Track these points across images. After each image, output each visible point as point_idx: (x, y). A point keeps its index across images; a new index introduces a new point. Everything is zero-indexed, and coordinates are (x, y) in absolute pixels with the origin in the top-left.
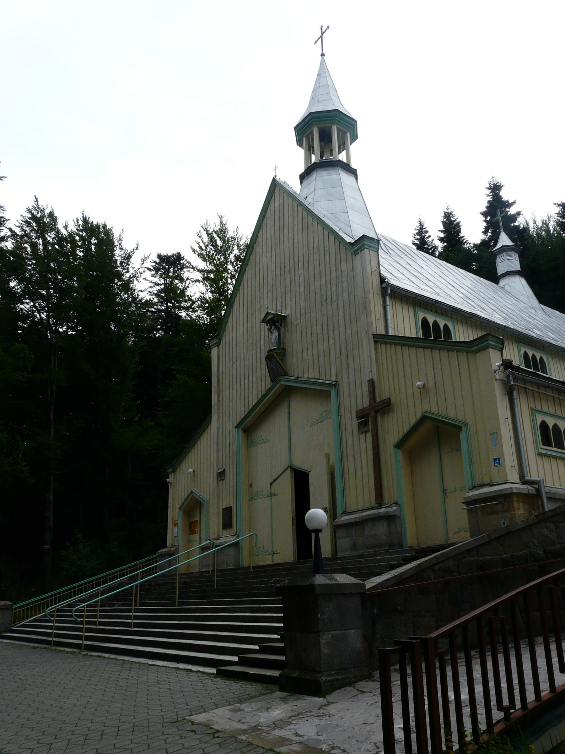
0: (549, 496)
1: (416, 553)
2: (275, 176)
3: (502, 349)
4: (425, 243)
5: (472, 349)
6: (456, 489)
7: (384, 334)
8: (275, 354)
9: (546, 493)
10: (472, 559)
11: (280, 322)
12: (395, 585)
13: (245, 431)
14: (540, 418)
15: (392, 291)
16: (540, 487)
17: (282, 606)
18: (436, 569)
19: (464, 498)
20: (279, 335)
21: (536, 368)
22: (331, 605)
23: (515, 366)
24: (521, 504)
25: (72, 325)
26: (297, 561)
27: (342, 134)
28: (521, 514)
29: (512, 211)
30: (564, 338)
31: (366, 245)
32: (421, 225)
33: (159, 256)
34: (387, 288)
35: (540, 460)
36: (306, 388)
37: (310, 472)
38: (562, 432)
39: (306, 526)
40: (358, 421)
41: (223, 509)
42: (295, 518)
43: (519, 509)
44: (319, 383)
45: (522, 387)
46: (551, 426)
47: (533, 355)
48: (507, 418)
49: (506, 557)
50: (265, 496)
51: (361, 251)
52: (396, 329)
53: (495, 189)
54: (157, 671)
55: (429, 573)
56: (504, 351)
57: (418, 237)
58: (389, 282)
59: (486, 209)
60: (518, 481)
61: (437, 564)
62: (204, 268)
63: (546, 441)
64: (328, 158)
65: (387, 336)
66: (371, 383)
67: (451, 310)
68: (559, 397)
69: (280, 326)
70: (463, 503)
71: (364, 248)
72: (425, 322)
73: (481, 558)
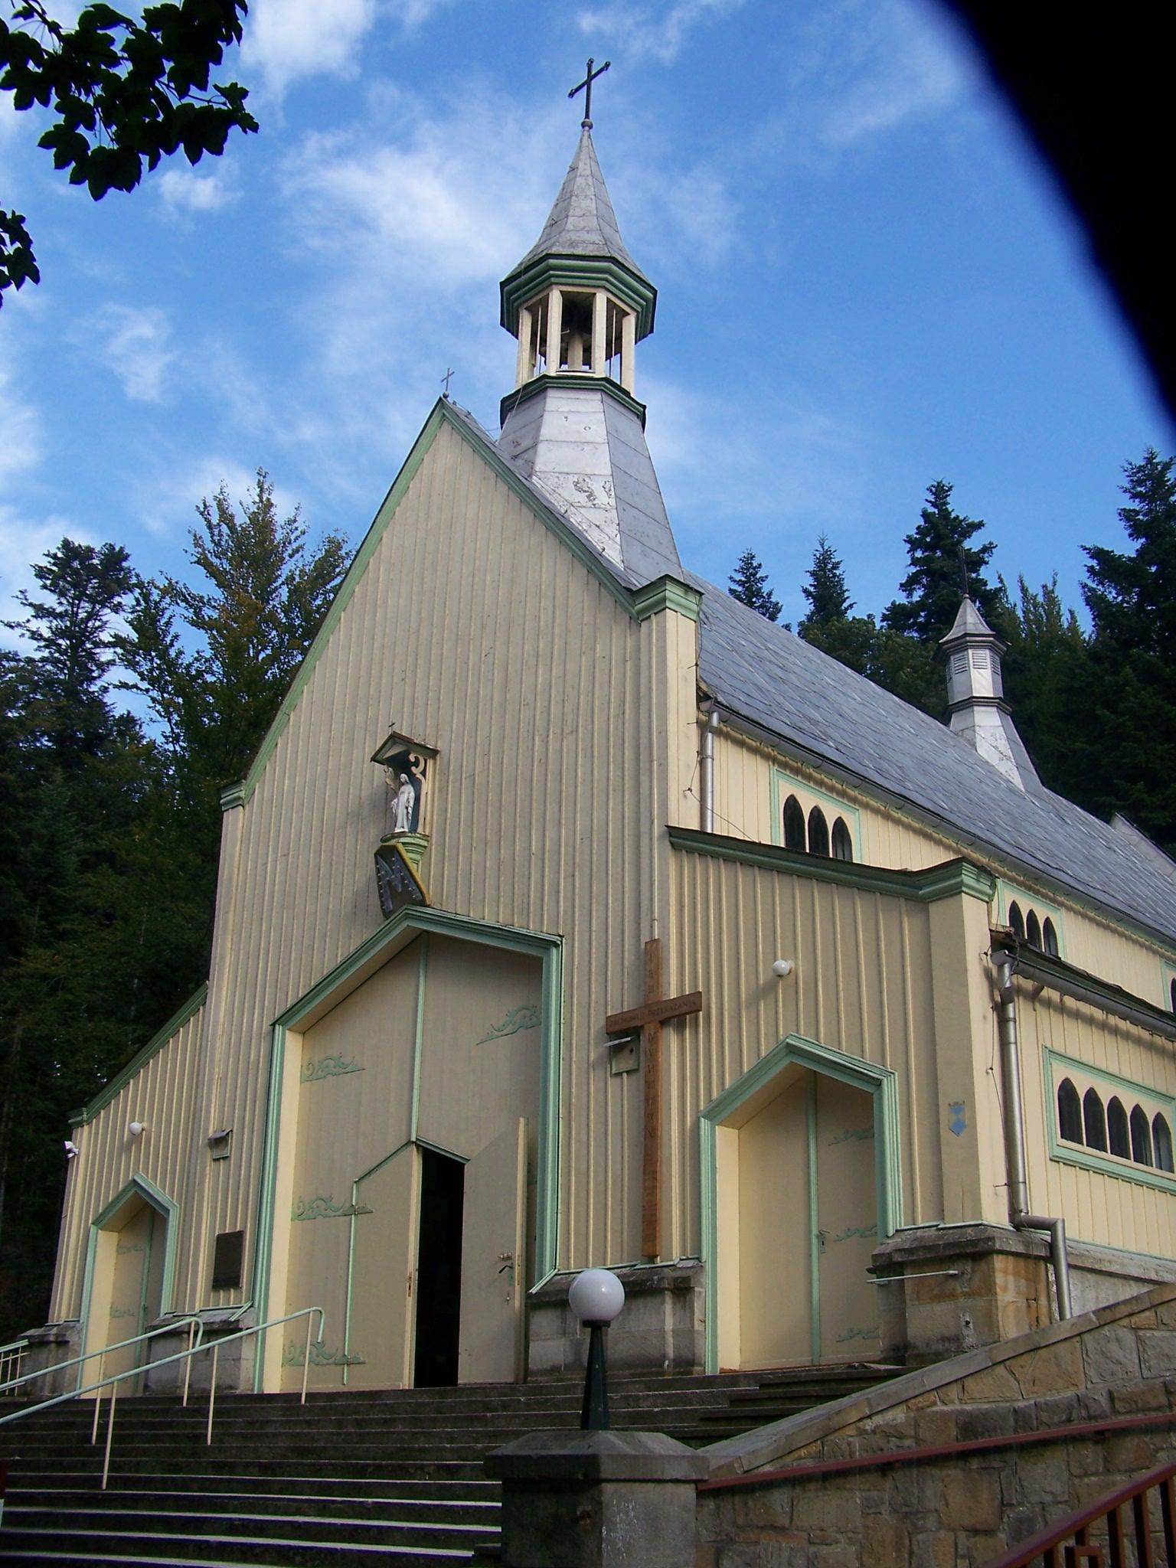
0: (1073, 1262)
1: (762, 1386)
2: (446, 396)
3: (991, 898)
4: (758, 593)
5: (920, 892)
6: (849, 1233)
8: (401, 847)
10: (945, 1408)
14: (1060, 1072)
16: (1054, 1236)
17: (500, 1504)
18: (866, 1431)
19: (874, 1256)
20: (417, 799)
22: (631, 1507)
24: (1011, 1279)
28: (1009, 1303)
29: (973, 544)
30: (1175, 907)
31: (672, 601)
32: (1085, 549)
36: (463, 941)
37: (468, 1160)
38: (1126, 1116)
40: (611, 1043)
43: (1005, 1289)
44: (534, 940)
47: (1031, 914)
48: (992, 1069)
49: (1025, 1406)
50: (338, 1213)
53: (940, 493)
55: (850, 1439)
56: (994, 904)
57: (739, 577)
59: (52, 129)
62: (177, 583)
63: (1069, 1130)
65: (701, 835)
69: (419, 776)
70: (870, 1271)
71: (663, 607)
72: (792, 808)
73: (968, 1407)
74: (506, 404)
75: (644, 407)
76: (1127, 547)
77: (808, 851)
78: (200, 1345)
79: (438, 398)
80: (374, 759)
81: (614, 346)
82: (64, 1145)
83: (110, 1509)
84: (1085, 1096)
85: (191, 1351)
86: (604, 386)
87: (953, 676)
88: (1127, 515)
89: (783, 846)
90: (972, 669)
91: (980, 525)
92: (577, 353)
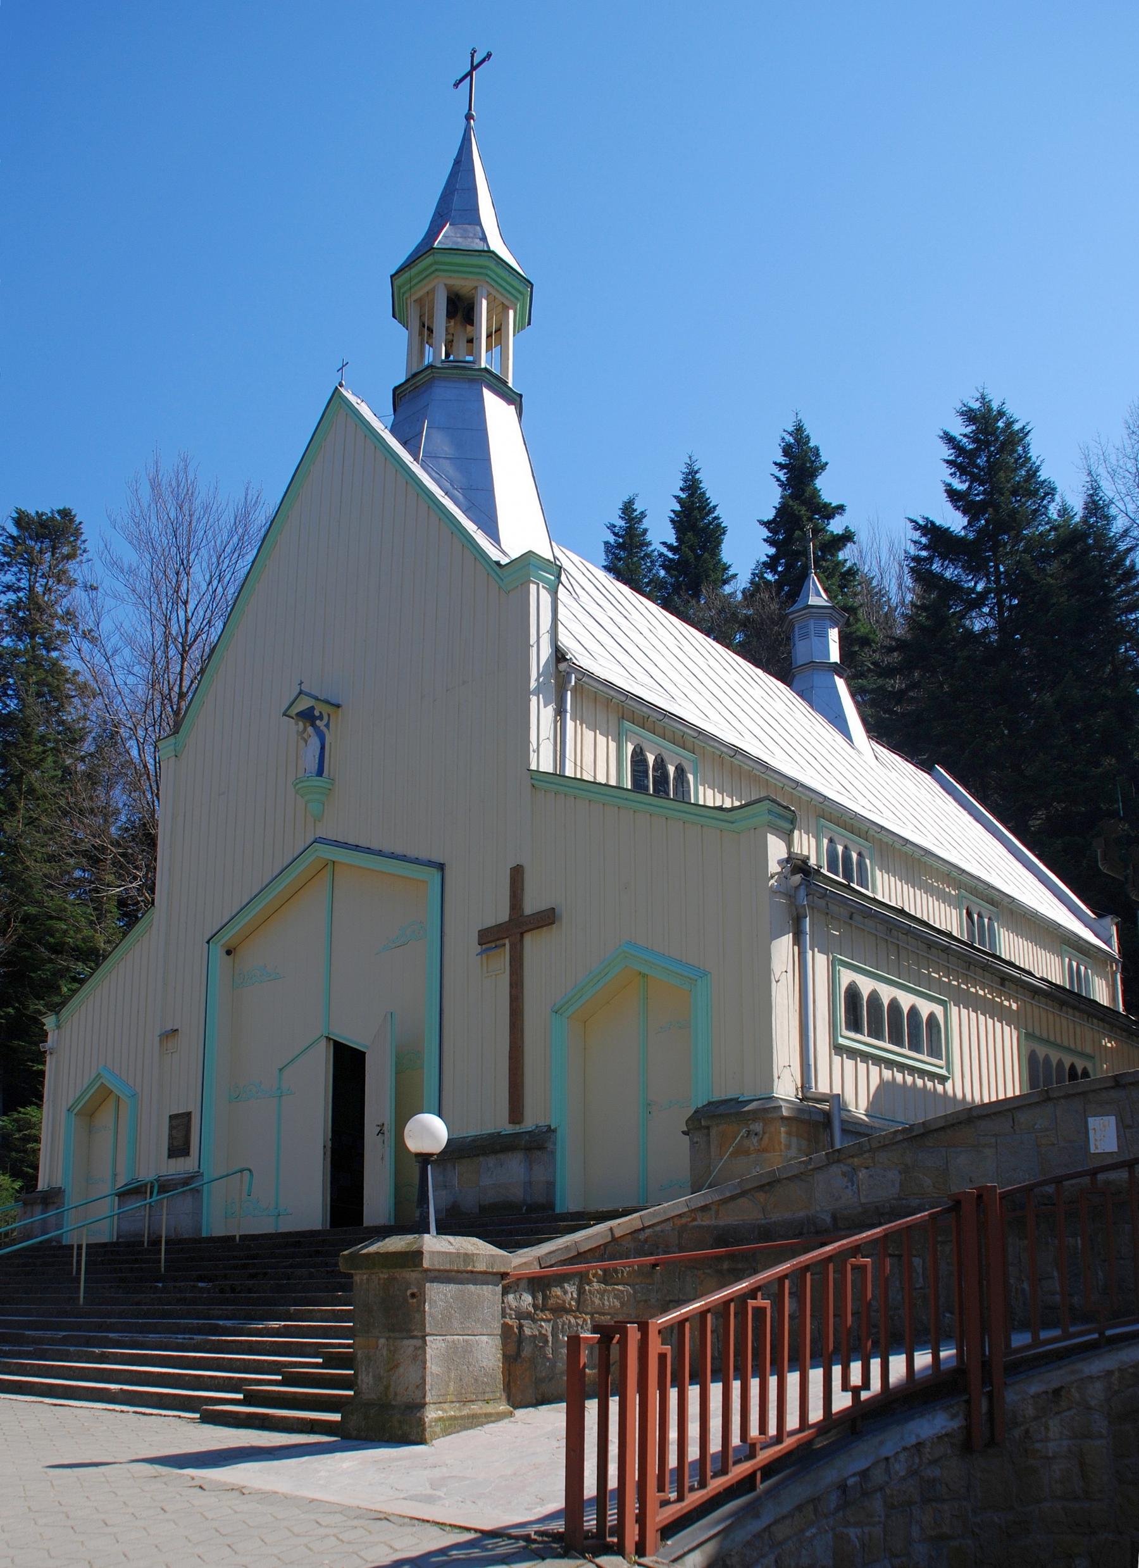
3: (792, 831)
7: (552, 772)
9: (843, 1122)
11: (325, 721)
12: (563, 1262)
13: (229, 953)
15: (578, 680)
21: (848, 875)
23: (814, 869)
25: (985, 994)
26: (328, 1228)
27: (499, 310)
33: (21, 520)
34: (569, 674)
35: (837, 1059)
39: (406, 1146)
41: (170, 1116)
42: (329, 1144)
45: (1029, 1002)
46: (865, 995)
48: (786, 972)
49: (767, 1223)
51: (521, 585)
52: (579, 763)
54: (6, 1440)
58: (575, 661)
60: (793, 1096)
61: (643, 1229)
64: (461, 359)
66: (517, 874)
67: (696, 735)
68: (887, 937)
69: (323, 728)
72: (639, 759)
74: (397, 393)
75: (521, 396)
76: (955, 521)
77: (651, 792)
78: (157, 1196)
79: (334, 388)
80: (285, 714)
81: (497, 334)
82: (591, 1397)
83: (158, 1372)
84: (909, 1011)
85: (148, 1201)
86: (484, 376)
87: (797, 643)
88: (953, 495)
89: (629, 787)
90: (812, 636)
91: (841, 508)
92: (461, 345)
